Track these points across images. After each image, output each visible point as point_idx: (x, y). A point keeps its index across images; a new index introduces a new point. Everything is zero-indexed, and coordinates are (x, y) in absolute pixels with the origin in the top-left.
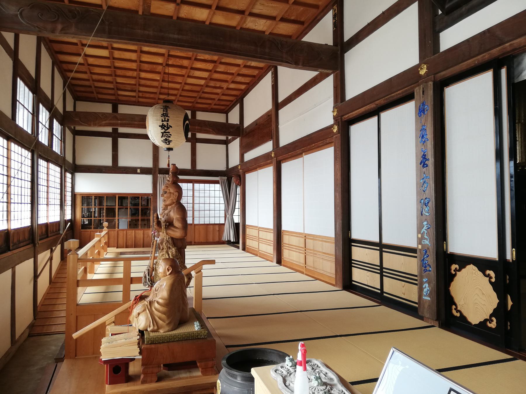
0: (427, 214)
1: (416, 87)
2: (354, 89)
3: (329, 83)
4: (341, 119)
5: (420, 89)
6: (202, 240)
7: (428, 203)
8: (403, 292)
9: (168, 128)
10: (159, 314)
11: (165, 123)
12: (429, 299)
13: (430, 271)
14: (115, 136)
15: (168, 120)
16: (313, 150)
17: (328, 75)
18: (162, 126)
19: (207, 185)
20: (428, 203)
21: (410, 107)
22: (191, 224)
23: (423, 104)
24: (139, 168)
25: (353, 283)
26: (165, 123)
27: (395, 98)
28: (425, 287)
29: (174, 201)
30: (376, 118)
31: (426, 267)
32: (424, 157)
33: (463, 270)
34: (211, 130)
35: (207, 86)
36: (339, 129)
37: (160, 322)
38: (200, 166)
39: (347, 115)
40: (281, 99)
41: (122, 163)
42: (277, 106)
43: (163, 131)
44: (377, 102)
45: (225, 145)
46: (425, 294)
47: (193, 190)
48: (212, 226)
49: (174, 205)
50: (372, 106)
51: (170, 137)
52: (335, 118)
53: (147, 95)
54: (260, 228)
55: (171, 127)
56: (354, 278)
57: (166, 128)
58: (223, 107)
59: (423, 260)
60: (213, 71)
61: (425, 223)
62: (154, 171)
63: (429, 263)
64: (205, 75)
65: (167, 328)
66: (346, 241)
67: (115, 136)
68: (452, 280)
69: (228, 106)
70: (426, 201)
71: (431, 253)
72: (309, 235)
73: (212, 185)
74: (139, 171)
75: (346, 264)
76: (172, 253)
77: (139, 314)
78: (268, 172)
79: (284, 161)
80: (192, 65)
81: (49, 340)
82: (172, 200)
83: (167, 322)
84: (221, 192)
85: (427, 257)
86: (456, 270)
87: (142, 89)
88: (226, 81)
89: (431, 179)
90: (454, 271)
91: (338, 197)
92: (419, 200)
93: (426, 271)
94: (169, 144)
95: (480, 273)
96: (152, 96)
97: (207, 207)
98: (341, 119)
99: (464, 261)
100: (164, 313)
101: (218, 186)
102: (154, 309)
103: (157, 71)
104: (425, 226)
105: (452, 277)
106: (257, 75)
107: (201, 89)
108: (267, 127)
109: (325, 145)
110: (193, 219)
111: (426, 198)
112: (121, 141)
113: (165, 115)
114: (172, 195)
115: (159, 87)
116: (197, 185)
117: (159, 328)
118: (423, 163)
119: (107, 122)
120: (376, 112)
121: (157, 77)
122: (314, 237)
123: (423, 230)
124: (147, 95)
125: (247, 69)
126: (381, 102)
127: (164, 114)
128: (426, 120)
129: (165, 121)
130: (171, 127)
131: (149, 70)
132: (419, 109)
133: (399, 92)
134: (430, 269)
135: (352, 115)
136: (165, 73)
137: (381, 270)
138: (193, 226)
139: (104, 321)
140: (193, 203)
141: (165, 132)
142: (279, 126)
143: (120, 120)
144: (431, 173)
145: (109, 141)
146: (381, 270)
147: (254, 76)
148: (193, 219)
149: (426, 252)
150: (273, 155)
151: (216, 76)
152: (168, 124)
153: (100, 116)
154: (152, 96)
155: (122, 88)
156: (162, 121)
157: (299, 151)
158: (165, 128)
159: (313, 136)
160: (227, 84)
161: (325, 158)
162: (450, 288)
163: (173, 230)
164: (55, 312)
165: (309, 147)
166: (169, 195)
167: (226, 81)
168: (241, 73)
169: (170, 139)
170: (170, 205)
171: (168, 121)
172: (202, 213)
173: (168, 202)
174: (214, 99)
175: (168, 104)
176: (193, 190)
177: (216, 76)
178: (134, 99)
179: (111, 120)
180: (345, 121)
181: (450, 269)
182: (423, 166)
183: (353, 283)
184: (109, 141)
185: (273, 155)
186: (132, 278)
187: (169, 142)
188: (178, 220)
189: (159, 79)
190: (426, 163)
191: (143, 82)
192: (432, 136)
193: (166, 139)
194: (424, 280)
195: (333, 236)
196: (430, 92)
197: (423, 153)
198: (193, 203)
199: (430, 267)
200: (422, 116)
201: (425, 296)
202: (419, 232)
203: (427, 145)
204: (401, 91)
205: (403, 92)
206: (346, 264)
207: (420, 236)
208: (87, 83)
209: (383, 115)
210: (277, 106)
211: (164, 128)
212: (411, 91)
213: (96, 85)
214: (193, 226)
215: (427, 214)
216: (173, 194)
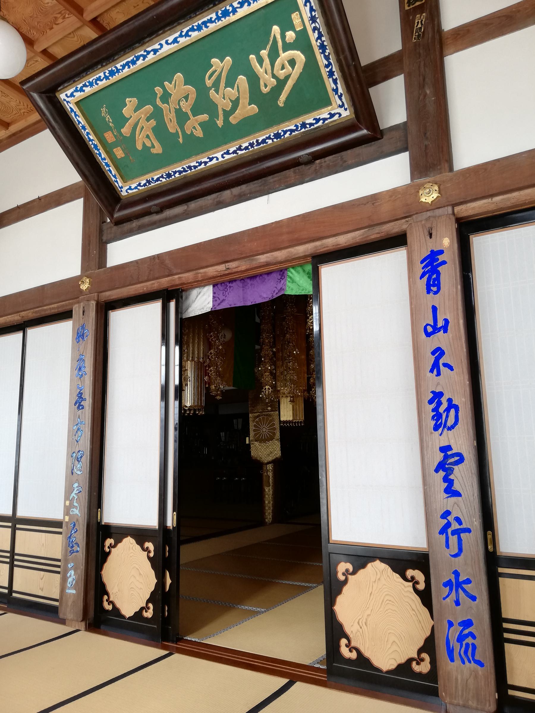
0: (79, 473)
5: (79, 307)
7: (81, 457)
13: (77, 551)
20: (81, 457)
28: (70, 576)
30: (19, 336)
31: (72, 547)
32: (80, 396)
44: (23, 314)
59: (70, 537)
61: (76, 485)
71: (81, 526)
85: (75, 532)
89: (87, 426)
93: (72, 552)
95: (345, 589)
105: (363, 660)
111: (79, 451)
118: (78, 403)
120: (21, 327)
123: (73, 494)
132: (78, 333)
133: (53, 306)
134: (78, 549)
149: (74, 525)
182: (78, 408)
190: (82, 403)
199: (78, 546)
201: (69, 589)
202: (67, 498)
203: (84, 380)
205: (58, 307)
207: (68, 503)
215: (79, 473)
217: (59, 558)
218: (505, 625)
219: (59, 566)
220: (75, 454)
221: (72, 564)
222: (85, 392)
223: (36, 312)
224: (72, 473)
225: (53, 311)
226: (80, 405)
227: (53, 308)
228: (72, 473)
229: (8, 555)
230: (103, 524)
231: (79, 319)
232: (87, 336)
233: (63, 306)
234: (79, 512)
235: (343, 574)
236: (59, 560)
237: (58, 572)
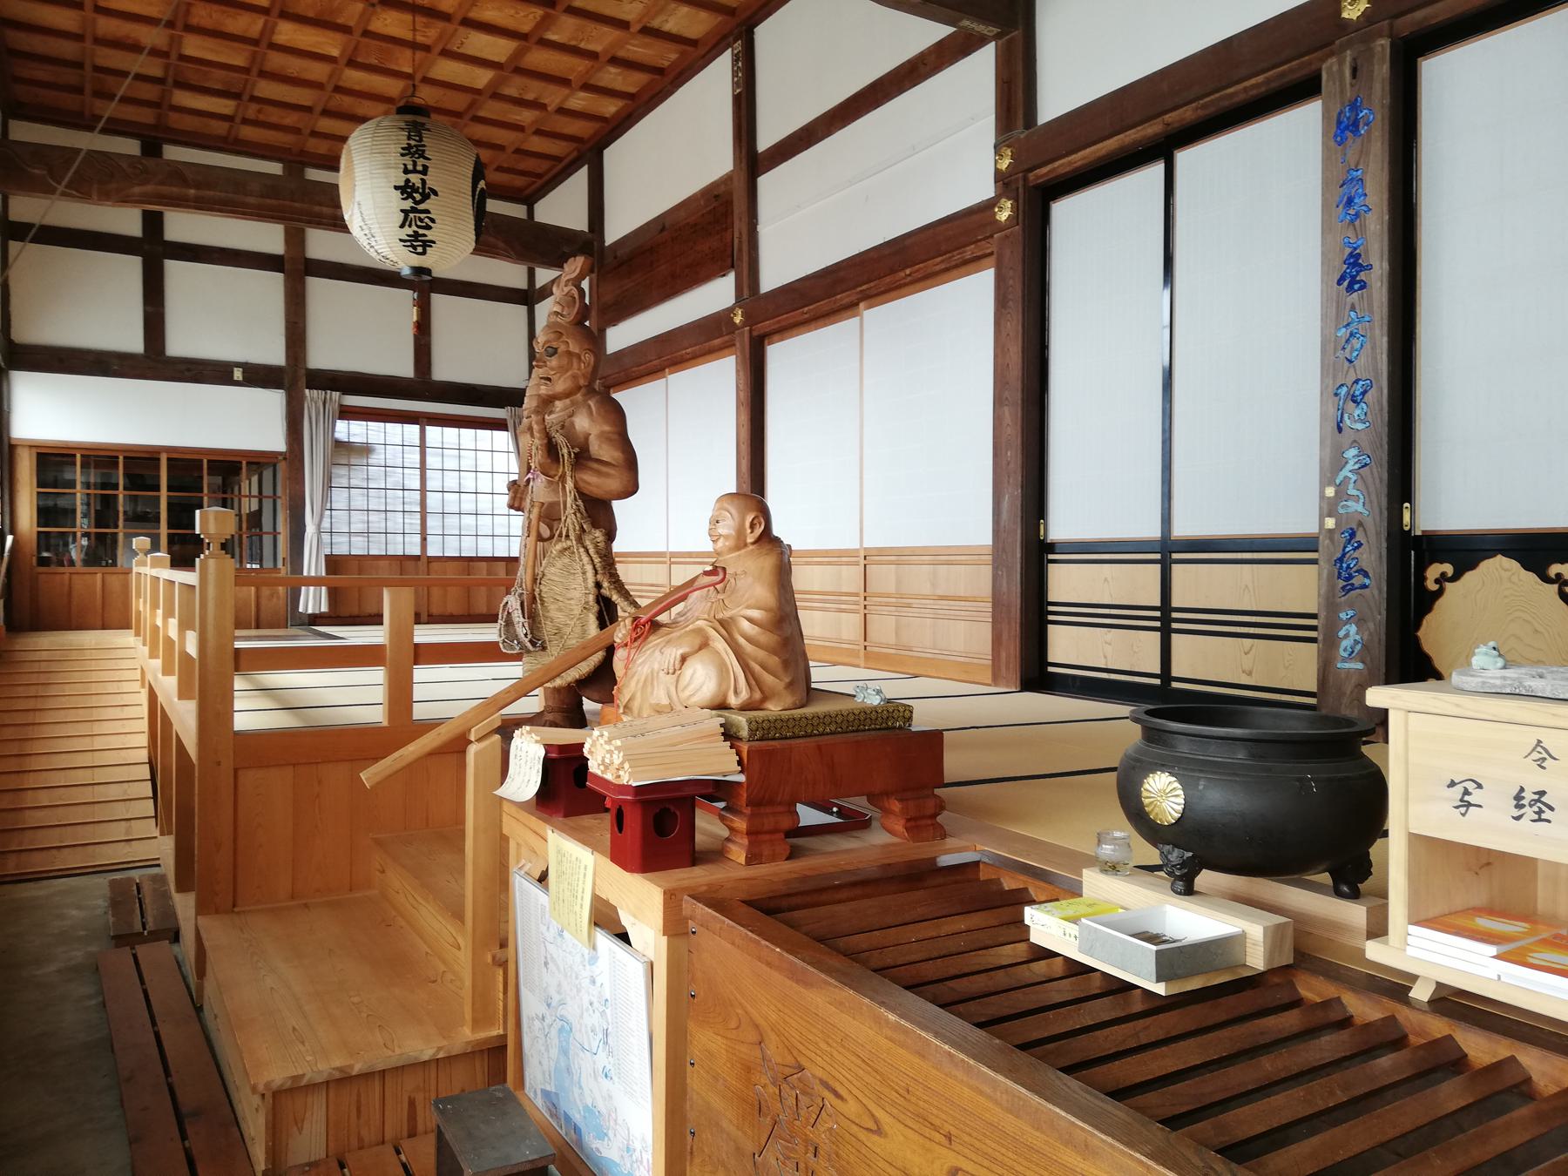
0: (1360, 426)
1: (1323, 60)
2: (1062, 91)
3: (981, 66)
4: (1025, 179)
5: (1341, 63)
6: (452, 608)
7: (1364, 393)
8: (1247, 668)
9: (425, 197)
10: (761, 654)
11: (415, 179)
12: (1360, 666)
13: (1364, 587)
14: (154, 251)
15: (425, 168)
16: (903, 291)
17: (981, 42)
18: (406, 190)
19: (467, 433)
20: (1364, 393)
21: (1306, 119)
22: (417, 558)
23: (1354, 107)
24: (238, 365)
25: (1051, 669)
26: (415, 179)
27: (1242, 97)
28: (1347, 636)
29: (582, 382)
30: (1157, 170)
31: (1350, 577)
32: (1355, 262)
33: (1469, 577)
34: (501, 245)
35: (496, 96)
36: (1015, 209)
37: (768, 679)
38: (444, 370)
39: (1045, 170)
40: (764, 142)
41: (179, 344)
42: (753, 161)
43: (408, 204)
44: (1167, 117)
45: (524, 308)
46: (1345, 655)
47: (423, 446)
48: (484, 564)
49: (579, 396)
50: (1152, 129)
51: (428, 227)
52: (999, 177)
53: (274, 115)
54: (673, 555)
55: (436, 194)
56: (1053, 656)
57: (418, 197)
58: (519, 181)
59: (1341, 560)
60: (535, 39)
61: (1353, 452)
62: (293, 378)
63: (1365, 565)
64: (499, 49)
65: (789, 700)
66: (1030, 549)
67: (154, 251)
68: (1429, 609)
69: (539, 176)
70: (1358, 389)
71: (1373, 538)
72: (881, 552)
73: (484, 434)
74: (238, 374)
75: (1031, 614)
76: (596, 546)
77: (684, 659)
78: (718, 378)
79: (776, 337)
80: (469, 10)
81: (41, 893)
82: (574, 377)
83: (787, 680)
84: (513, 457)
85: (1355, 549)
86: (1442, 579)
87: (266, 89)
88: (564, 82)
89: (1377, 324)
90: (1437, 581)
91: (1008, 419)
92: (1331, 390)
93: (1348, 589)
94: (424, 253)
95: (1531, 577)
96: (291, 119)
97: (468, 503)
98: (1025, 179)
99: (1466, 551)
100: (773, 651)
101: (502, 438)
102: (742, 641)
103: (340, 21)
104: (1351, 462)
105: (1427, 601)
106: (673, 64)
107: (471, 106)
108: (711, 231)
109: (957, 266)
110: (424, 540)
111: (1356, 382)
112: (175, 270)
113: (414, 151)
114: (575, 361)
115: (330, 87)
116: (433, 432)
117: (765, 699)
118: (1351, 274)
119: (149, 188)
120: (1163, 150)
121: (331, 44)
122: (899, 556)
123: (1345, 472)
124: (274, 115)
125: (648, 40)
126: (1187, 114)
127: (409, 147)
128: (1364, 152)
129: (415, 171)
130: (436, 194)
131: (311, 14)
132: (1339, 122)
133: (1253, 81)
134: (1367, 581)
135: (1070, 163)
136: (367, 33)
137: (1166, 620)
138: (422, 564)
139: (460, 730)
140: (423, 490)
141: (414, 210)
142: (759, 228)
143: (198, 186)
144: (1376, 304)
145: (132, 267)
146: (1166, 620)
147: (659, 71)
148: (424, 540)
149: (1353, 534)
150: (738, 319)
151: (539, 59)
152: (424, 182)
153: (124, 165)
154: (291, 119)
155: (194, 78)
156: (406, 171)
157: (843, 298)
158: (414, 193)
159: (908, 242)
160: (566, 91)
161: (968, 303)
162: (1419, 634)
163: (599, 473)
164: (28, 813)
165: (888, 279)
166: (565, 361)
167: (564, 82)
168: (621, 54)
169: (430, 235)
170: (567, 395)
171: (425, 171)
172: (452, 521)
173: (561, 385)
174: (501, 148)
175: (420, 119)
176: (423, 446)
177: (539, 59)
178: (220, 128)
179: (162, 183)
180: (1037, 187)
181: (1425, 579)
182: (1350, 289)
183: (1051, 669)
184: (132, 267)
185: (738, 319)
186: (417, 645)
187: (427, 244)
188: (609, 440)
189: (335, 53)
190: (1362, 276)
191: (276, 61)
192: (1386, 196)
193: (416, 235)
194: (1343, 616)
195: (986, 538)
196: (1382, 70)
197: (1348, 251)
198: (423, 490)
199: (1366, 575)
200: (1350, 141)
201: (1344, 660)
202: (1326, 480)
203: (1363, 226)
204: (1260, 79)
205: (1268, 81)
206: (1031, 614)
207: (1330, 492)
208: (68, 49)
209: (1185, 158)
210: (753, 161)
211: (410, 196)
212: (1314, 67)
213: (101, 62)
214: (422, 564)
215: (1360, 426)
216: (579, 357)
217: (1315, 611)
218: (1051, 608)
219: (1314, 628)
220: (1345, 389)
221: (1351, 613)
222: (1367, 252)
223: (1204, 107)
224: (1340, 430)
225: (1254, 92)
226: (1353, 281)
227: (1253, 87)
228: (1340, 430)
229: (1175, 626)
230: (1419, 533)
231: (1342, 91)
232: (1367, 124)
233: (1282, 74)
234: (1362, 506)
235: (1437, 581)
236: (1314, 616)
237: (1313, 640)
